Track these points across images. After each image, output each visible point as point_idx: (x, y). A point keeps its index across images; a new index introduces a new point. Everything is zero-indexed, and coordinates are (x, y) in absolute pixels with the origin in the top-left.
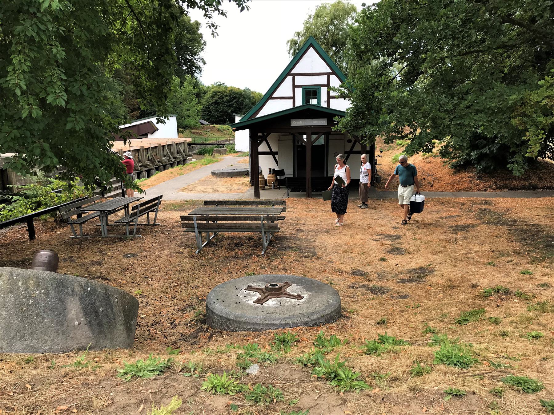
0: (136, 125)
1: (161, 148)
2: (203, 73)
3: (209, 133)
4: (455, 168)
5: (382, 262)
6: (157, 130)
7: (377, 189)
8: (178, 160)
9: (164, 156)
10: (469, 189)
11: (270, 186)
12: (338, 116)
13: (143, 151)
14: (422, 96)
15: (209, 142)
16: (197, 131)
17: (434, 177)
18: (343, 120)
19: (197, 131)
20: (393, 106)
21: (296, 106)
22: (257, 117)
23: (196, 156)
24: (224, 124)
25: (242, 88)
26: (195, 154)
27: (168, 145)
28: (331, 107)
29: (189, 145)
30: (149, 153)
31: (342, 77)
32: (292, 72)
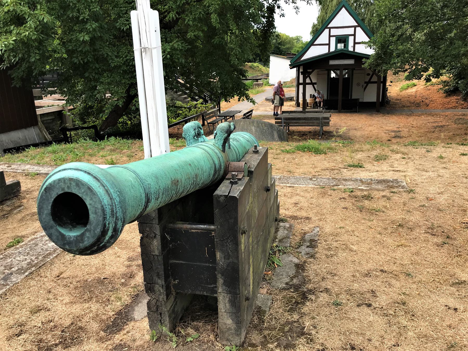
4: (447, 92)
5: (389, 142)
7: (387, 108)
10: (455, 107)
11: (310, 106)
12: (365, 58)
14: (417, 47)
17: (431, 99)
18: (369, 61)
20: (399, 54)
21: (331, 51)
22: (302, 59)
24: (255, 62)
28: (356, 51)
31: (370, 34)
32: (328, 26)
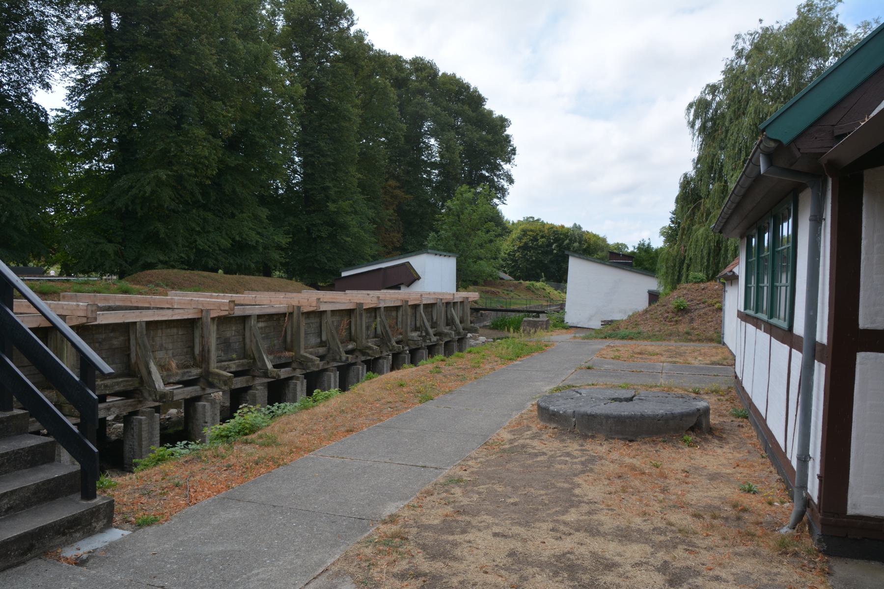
0: (381, 269)
1: (409, 310)
2: (508, 198)
3: (512, 294)
6: (419, 278)
8: (447, 339)
9: (416, 329)
13: (361, 315)
15: (513, 307)
16: (493, 289)
19: (493, 289)
23: (487, 331)
24: (538, 281)
25: (569, 225)
26: (485, 327)
27: (427, 306)
29: (475, 310)
30: (378, 319)
